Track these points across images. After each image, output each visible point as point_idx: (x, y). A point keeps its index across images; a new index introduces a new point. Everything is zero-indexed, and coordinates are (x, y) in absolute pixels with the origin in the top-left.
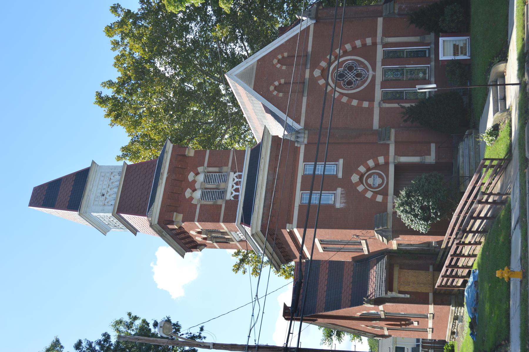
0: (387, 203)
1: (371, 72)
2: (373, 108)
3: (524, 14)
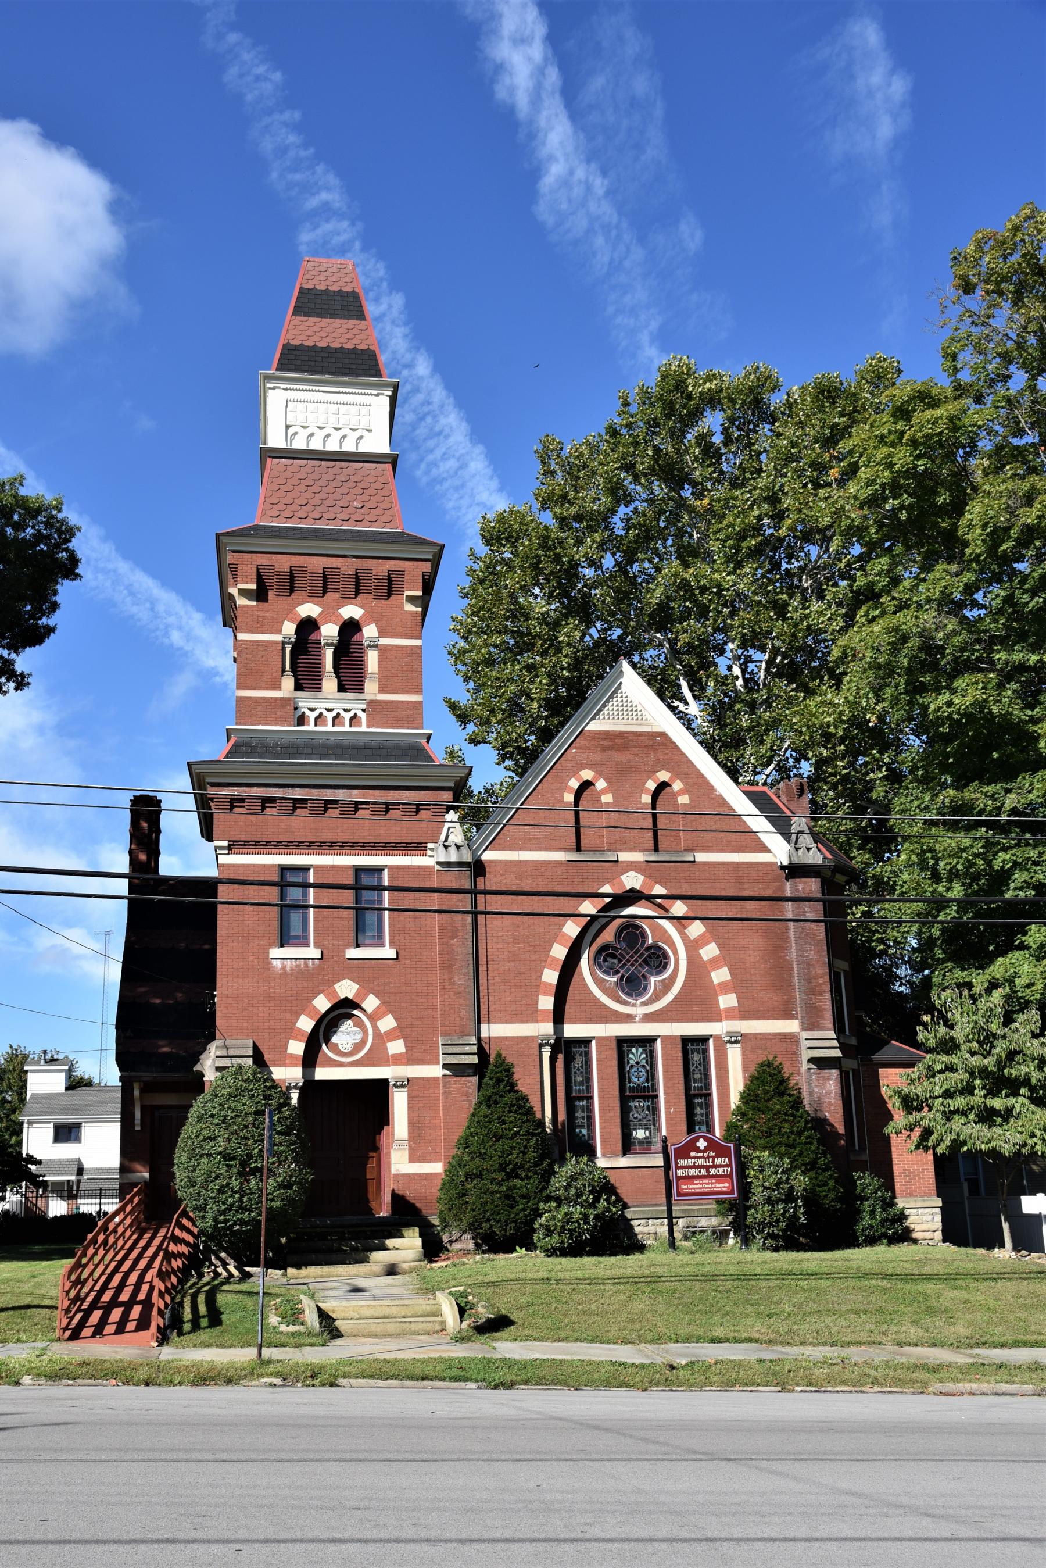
0: (285, 1065)
1: (640, 1011)
2: (537, 1022)
3: (539, 1452)
